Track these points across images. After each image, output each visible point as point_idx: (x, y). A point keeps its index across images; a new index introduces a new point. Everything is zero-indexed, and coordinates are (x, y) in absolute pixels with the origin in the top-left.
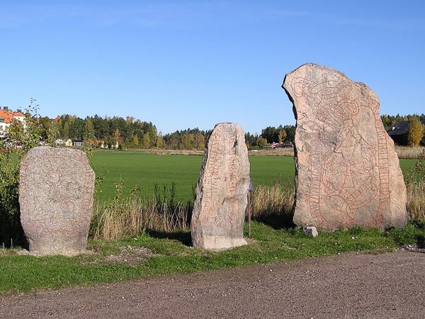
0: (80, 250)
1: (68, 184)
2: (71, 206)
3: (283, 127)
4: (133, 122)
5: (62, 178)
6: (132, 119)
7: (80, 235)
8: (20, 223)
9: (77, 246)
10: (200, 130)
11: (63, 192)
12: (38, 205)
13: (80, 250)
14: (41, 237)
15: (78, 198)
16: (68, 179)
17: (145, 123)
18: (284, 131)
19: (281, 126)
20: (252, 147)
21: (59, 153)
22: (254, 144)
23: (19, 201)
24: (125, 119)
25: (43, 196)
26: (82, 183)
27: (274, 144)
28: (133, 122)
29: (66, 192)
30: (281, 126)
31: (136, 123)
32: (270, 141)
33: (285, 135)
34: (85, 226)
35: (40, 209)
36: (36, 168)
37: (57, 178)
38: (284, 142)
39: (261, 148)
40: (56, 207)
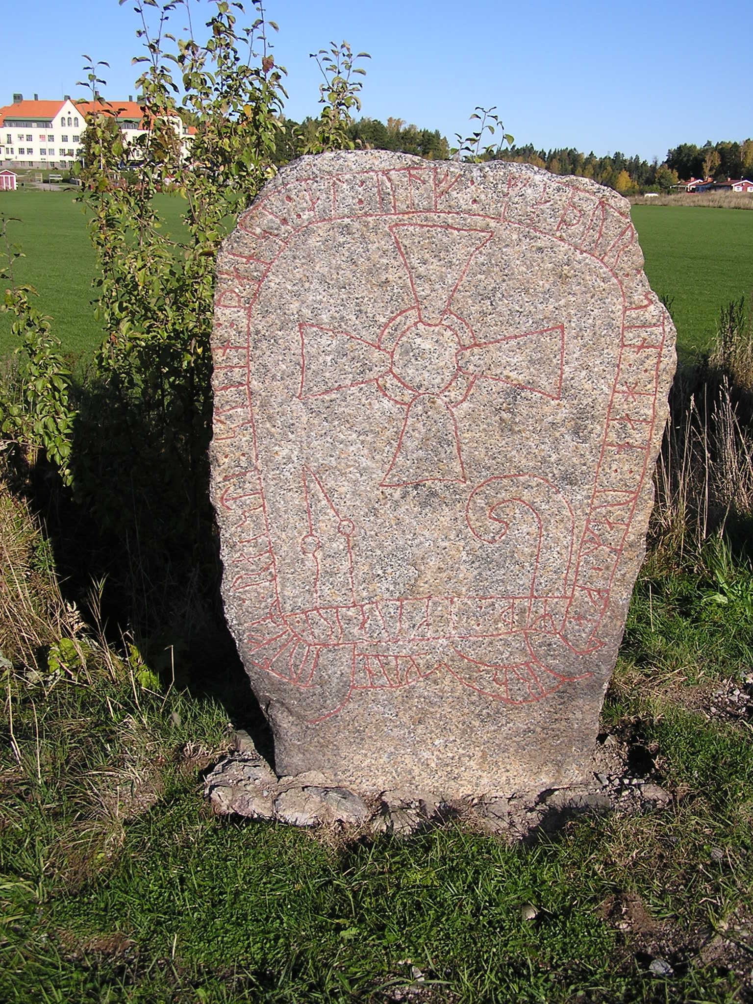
0: (559, 765)
1: (515, 391)
2: (526, 528)
3: (714, 144)
4: (401, 131)
5: (475, 359)
6: (399, 123)
7: (566, 689)
8: (216, 604)
9: (544, 744)
10: (537, 148)
11: (478, 440)
12: (326, 524)
13: (559, 765)
14: (344, 699)
15: (569, 479)
16: (514, 363)
17: (426, 132)
18: (716, 154)
19: (709, 143)
20: (647, 187)
21: (462, 198)
22: (650, 182)
23: (216, 495)
24: (385, 124)
25: (359, 466)
26: (598, 390)
27: (693, 183)
28: (401, 131)
29: (498, 441)
30: (709, 143)
31: (407, 132)
32: (685, 176)
33: (718, 162)
34: (596, 641)
35: (339, 545)
36: (316, 294)
37: (448, 357)
38: (714, 177)
39: (666, 190)
40: (434, 534)
